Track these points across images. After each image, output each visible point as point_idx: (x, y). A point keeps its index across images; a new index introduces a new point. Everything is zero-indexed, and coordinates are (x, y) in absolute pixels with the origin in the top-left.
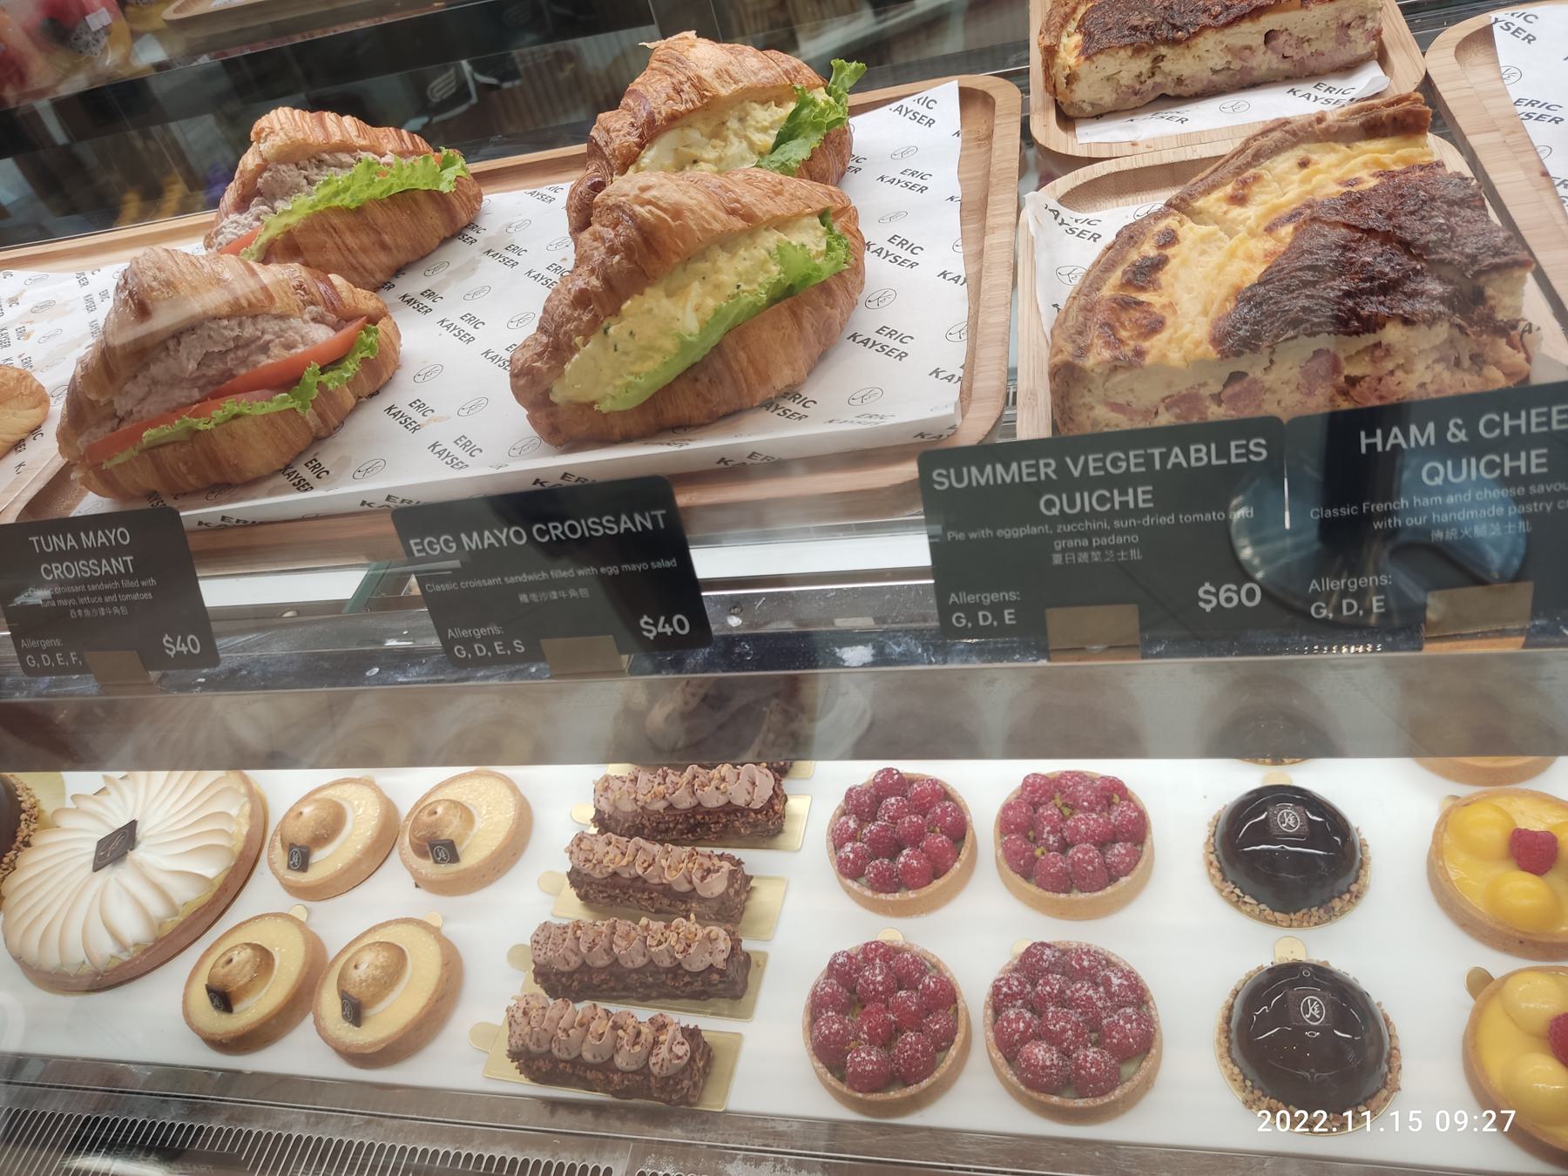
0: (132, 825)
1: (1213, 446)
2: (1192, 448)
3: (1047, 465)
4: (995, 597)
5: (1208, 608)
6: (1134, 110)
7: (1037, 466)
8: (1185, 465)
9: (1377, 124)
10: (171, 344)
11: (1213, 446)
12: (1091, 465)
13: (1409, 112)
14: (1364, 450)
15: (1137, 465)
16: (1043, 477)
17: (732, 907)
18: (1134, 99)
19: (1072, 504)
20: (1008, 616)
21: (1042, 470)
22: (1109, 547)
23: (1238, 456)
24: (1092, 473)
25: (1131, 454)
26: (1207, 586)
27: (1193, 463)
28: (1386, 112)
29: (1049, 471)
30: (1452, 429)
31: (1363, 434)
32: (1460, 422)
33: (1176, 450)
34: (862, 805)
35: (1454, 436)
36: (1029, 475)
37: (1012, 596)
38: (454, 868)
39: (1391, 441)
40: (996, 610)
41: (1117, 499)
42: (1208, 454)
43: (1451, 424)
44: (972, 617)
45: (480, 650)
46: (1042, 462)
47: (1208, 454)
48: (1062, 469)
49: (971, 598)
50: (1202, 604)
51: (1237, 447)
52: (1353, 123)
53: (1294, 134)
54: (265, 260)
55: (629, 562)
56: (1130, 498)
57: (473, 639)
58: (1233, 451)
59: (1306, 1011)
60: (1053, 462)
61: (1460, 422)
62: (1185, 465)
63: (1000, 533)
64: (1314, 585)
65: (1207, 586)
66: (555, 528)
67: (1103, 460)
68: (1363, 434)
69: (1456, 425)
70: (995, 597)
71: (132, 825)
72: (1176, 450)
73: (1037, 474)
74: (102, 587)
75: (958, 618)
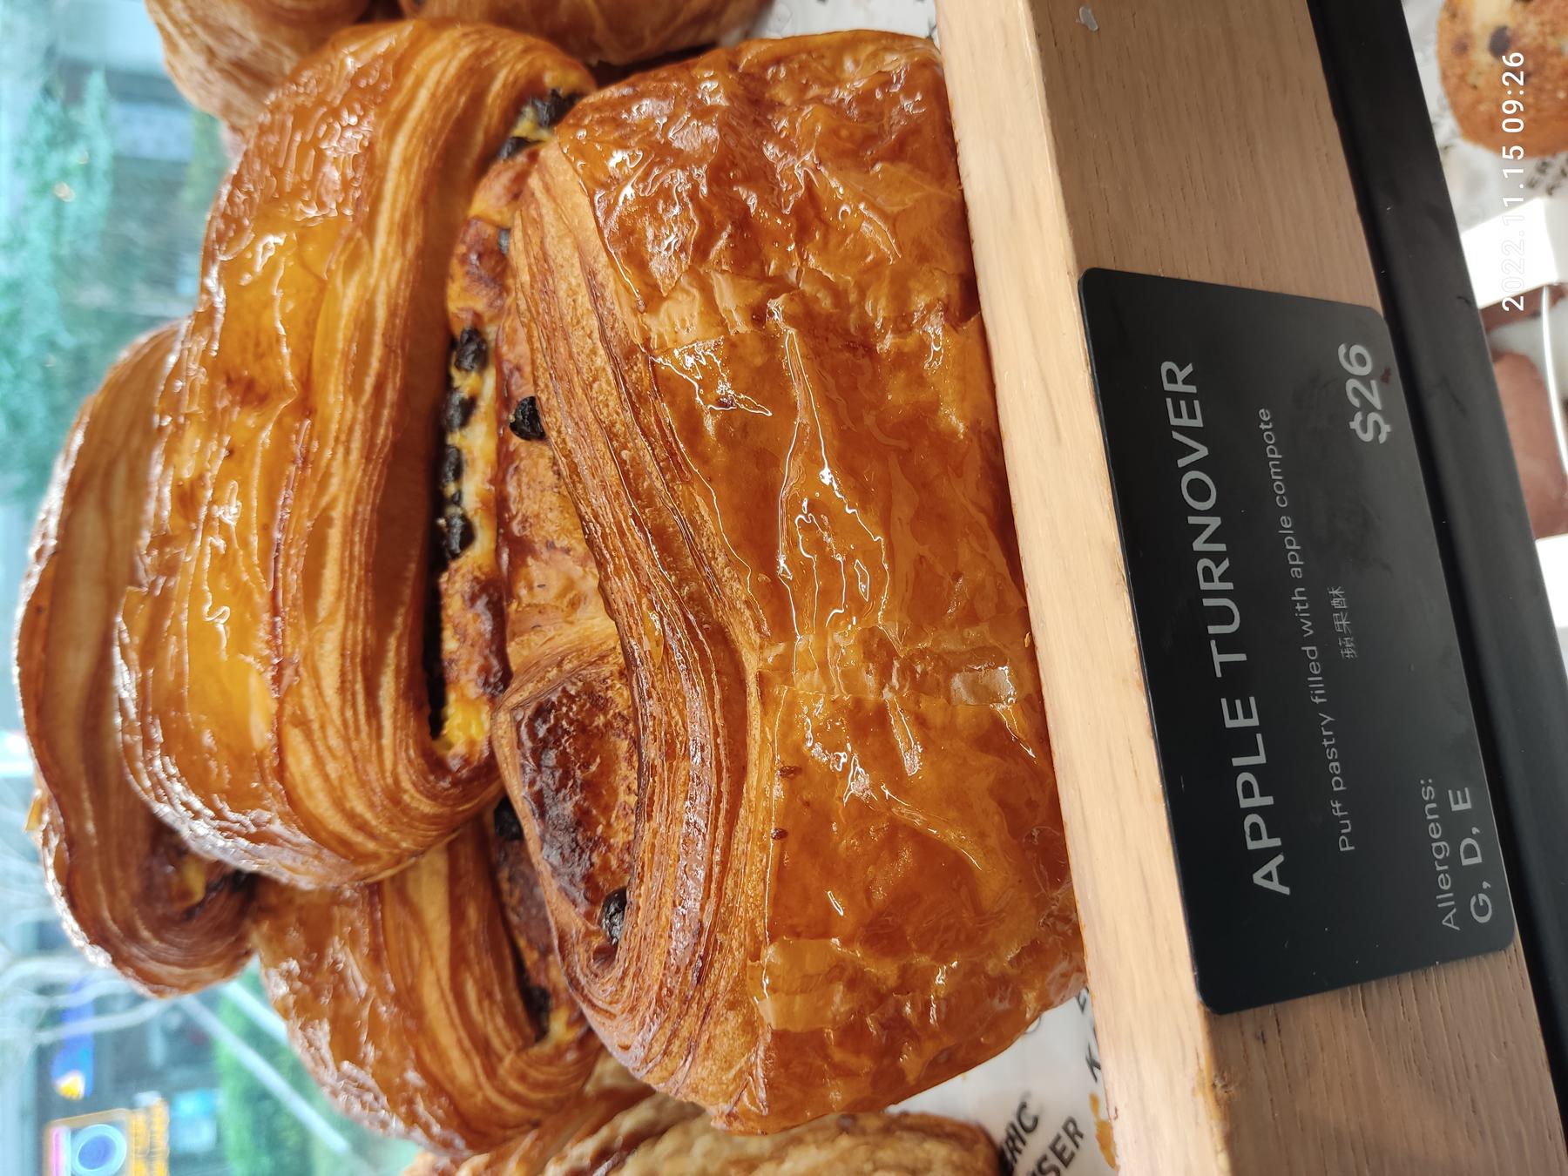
0: (542, 436)
1: (1252, 700)
3: (1172, 377)
4: (1446, 899)
5: (1386, 428)
6: (958, 224)
7: (1176, 396)
8: (1280, 859)
10: (463, 299)
11: (1252, 700)
12: (1185, 421)
14: (1286, 890)
15: (1248, 715)
16: (1192, 389)
21: (1180, 387)
23: (1248, 715)
24: (1198, 422)
29: (1181, 375)
36: (1192, 416)
38: (277, 282)
50: (1383, 438)
51: (1457, 802)
54: (542, 1033)
58: (1241, 722)
60: (1167, 366)
62: (1280, 859)
63: (1296, 573)
64: (1449, 922)
71: (542, 436)
73: (1189, 398)
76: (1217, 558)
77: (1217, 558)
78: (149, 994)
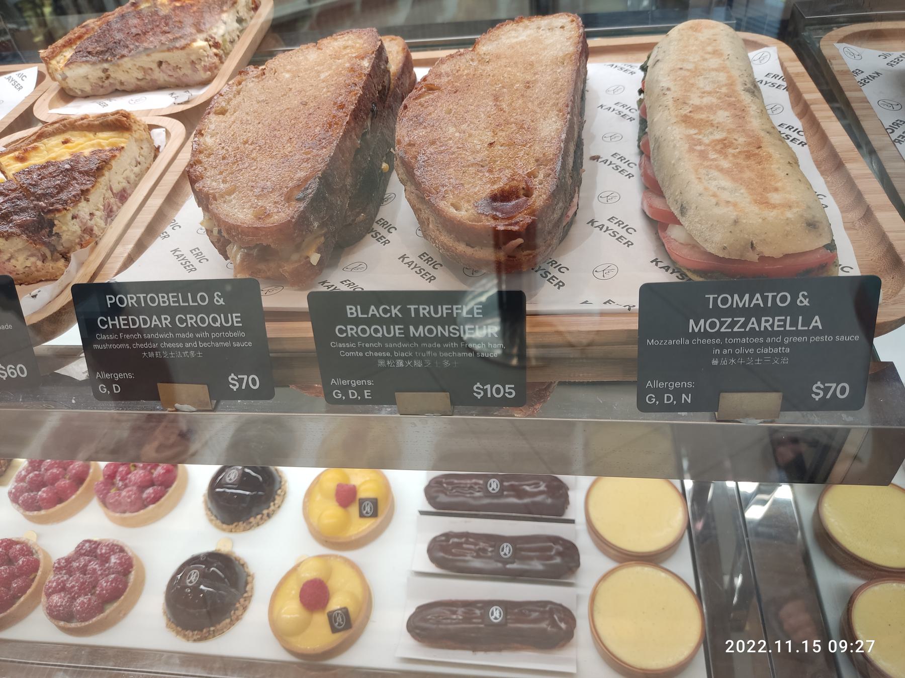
1: (359, 307)
2: (763, 319)
4: (360, 383)
8: (757, 329)
11: (359, 307)
13: (117, 120)
17: (447, 554)
18: (101, 90)
19: (389, 332)
20: (366, 393)
22: (768, 354)
26: (478, 385)
28: (111, 118)
30: (801, 298)
32: (806, 294)
33: (753, 319)
35: (801, 302)
36: (779, 326)
37: (690, 385)
39: (754, 302)
40: (677, 393)
41: (110, 323)
42: (356, 311)
44: (345, 394)
45: (353, 394)
47: (356, 311)
49: (344, 383)
50: (813, 396)
52: (96, 123)
53: (65, 126)
55: (125, 349)
56: (117, 322)
57: (349, 387)
59: (492, 614)
61: (806, 294)
62: (757, 329)
65: (478, 385)
66: (191, 318)
69: (803, 295)
70: (360, 383)
72: (753, 319)
74: (230, 334)
75: (336, 393)
76: (772, 326)
77: (772, 326)
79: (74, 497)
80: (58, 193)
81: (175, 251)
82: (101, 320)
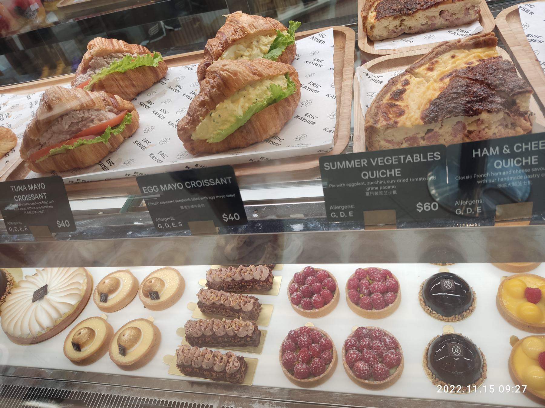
0: (46, 286)
1: (422, 155)
3: (364, 161)
4: (346, 207)
5: (420, 211)
7: (360, 162)
8: (412, 161)
9: (479, 43)
11: (422, 155)
12: (379, 161)
13: (490, 39)
14: (474, 156)
15: (395, 161)
16: (362, 165)
19: (373, 175)
20: (350, 214)
21: (362, 163)
22: (385, 190)
23: (430, 158)
24: (380, 164)
25: (393, 157)
26: (420, 203)
27: (415, 161)
28: (482, 39)
29: (365, 163)
30: (505, 149)
31: (474, 151)
32: (507, 146)
34: (300, 279)
35: (505, 151)
37: (352, 207)
39: (483, 153)
40: (346, 211)
42: (420, 157)
43: (504, 147)
44: (338, 214)
45: (167, 226)
46: (362, 160)
47: (420, 157)
48: (369, 163)
49: (338, 208)
50: (418, 210)
51: (430, 155)
52: (470, 43)
53: (450, 46)
55: (219, 195)
57: (164, 222)
58: (429, 157)
60: (366, 160)
61: (507, 146)
62: (412, 161)
63: (348, 185)
64: (457, 203)
65: (420, 203)
66: (193, 183)
67: (383, 160)
68: (474, 151)
69: (506, 147)
70: (346, 207)
71: (46, 286)
73: (361, 164)
74: (35, 204)
75: (333, 215)
78: (156, 59)
79: (333, 300)
80: (494, 72)
81: (151, 155)
82: (187, 184)
